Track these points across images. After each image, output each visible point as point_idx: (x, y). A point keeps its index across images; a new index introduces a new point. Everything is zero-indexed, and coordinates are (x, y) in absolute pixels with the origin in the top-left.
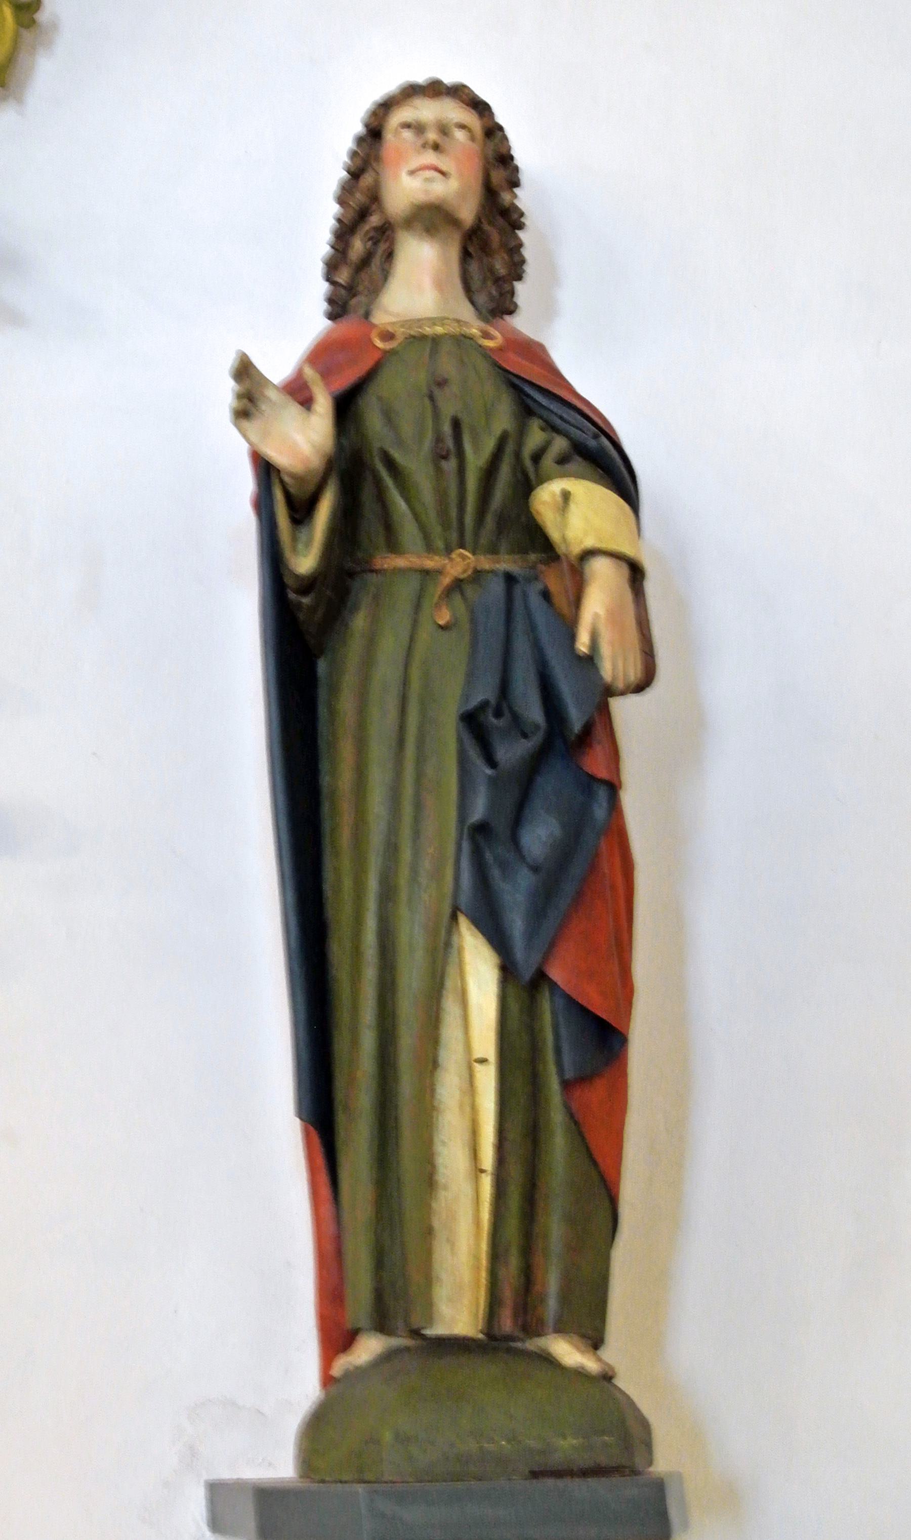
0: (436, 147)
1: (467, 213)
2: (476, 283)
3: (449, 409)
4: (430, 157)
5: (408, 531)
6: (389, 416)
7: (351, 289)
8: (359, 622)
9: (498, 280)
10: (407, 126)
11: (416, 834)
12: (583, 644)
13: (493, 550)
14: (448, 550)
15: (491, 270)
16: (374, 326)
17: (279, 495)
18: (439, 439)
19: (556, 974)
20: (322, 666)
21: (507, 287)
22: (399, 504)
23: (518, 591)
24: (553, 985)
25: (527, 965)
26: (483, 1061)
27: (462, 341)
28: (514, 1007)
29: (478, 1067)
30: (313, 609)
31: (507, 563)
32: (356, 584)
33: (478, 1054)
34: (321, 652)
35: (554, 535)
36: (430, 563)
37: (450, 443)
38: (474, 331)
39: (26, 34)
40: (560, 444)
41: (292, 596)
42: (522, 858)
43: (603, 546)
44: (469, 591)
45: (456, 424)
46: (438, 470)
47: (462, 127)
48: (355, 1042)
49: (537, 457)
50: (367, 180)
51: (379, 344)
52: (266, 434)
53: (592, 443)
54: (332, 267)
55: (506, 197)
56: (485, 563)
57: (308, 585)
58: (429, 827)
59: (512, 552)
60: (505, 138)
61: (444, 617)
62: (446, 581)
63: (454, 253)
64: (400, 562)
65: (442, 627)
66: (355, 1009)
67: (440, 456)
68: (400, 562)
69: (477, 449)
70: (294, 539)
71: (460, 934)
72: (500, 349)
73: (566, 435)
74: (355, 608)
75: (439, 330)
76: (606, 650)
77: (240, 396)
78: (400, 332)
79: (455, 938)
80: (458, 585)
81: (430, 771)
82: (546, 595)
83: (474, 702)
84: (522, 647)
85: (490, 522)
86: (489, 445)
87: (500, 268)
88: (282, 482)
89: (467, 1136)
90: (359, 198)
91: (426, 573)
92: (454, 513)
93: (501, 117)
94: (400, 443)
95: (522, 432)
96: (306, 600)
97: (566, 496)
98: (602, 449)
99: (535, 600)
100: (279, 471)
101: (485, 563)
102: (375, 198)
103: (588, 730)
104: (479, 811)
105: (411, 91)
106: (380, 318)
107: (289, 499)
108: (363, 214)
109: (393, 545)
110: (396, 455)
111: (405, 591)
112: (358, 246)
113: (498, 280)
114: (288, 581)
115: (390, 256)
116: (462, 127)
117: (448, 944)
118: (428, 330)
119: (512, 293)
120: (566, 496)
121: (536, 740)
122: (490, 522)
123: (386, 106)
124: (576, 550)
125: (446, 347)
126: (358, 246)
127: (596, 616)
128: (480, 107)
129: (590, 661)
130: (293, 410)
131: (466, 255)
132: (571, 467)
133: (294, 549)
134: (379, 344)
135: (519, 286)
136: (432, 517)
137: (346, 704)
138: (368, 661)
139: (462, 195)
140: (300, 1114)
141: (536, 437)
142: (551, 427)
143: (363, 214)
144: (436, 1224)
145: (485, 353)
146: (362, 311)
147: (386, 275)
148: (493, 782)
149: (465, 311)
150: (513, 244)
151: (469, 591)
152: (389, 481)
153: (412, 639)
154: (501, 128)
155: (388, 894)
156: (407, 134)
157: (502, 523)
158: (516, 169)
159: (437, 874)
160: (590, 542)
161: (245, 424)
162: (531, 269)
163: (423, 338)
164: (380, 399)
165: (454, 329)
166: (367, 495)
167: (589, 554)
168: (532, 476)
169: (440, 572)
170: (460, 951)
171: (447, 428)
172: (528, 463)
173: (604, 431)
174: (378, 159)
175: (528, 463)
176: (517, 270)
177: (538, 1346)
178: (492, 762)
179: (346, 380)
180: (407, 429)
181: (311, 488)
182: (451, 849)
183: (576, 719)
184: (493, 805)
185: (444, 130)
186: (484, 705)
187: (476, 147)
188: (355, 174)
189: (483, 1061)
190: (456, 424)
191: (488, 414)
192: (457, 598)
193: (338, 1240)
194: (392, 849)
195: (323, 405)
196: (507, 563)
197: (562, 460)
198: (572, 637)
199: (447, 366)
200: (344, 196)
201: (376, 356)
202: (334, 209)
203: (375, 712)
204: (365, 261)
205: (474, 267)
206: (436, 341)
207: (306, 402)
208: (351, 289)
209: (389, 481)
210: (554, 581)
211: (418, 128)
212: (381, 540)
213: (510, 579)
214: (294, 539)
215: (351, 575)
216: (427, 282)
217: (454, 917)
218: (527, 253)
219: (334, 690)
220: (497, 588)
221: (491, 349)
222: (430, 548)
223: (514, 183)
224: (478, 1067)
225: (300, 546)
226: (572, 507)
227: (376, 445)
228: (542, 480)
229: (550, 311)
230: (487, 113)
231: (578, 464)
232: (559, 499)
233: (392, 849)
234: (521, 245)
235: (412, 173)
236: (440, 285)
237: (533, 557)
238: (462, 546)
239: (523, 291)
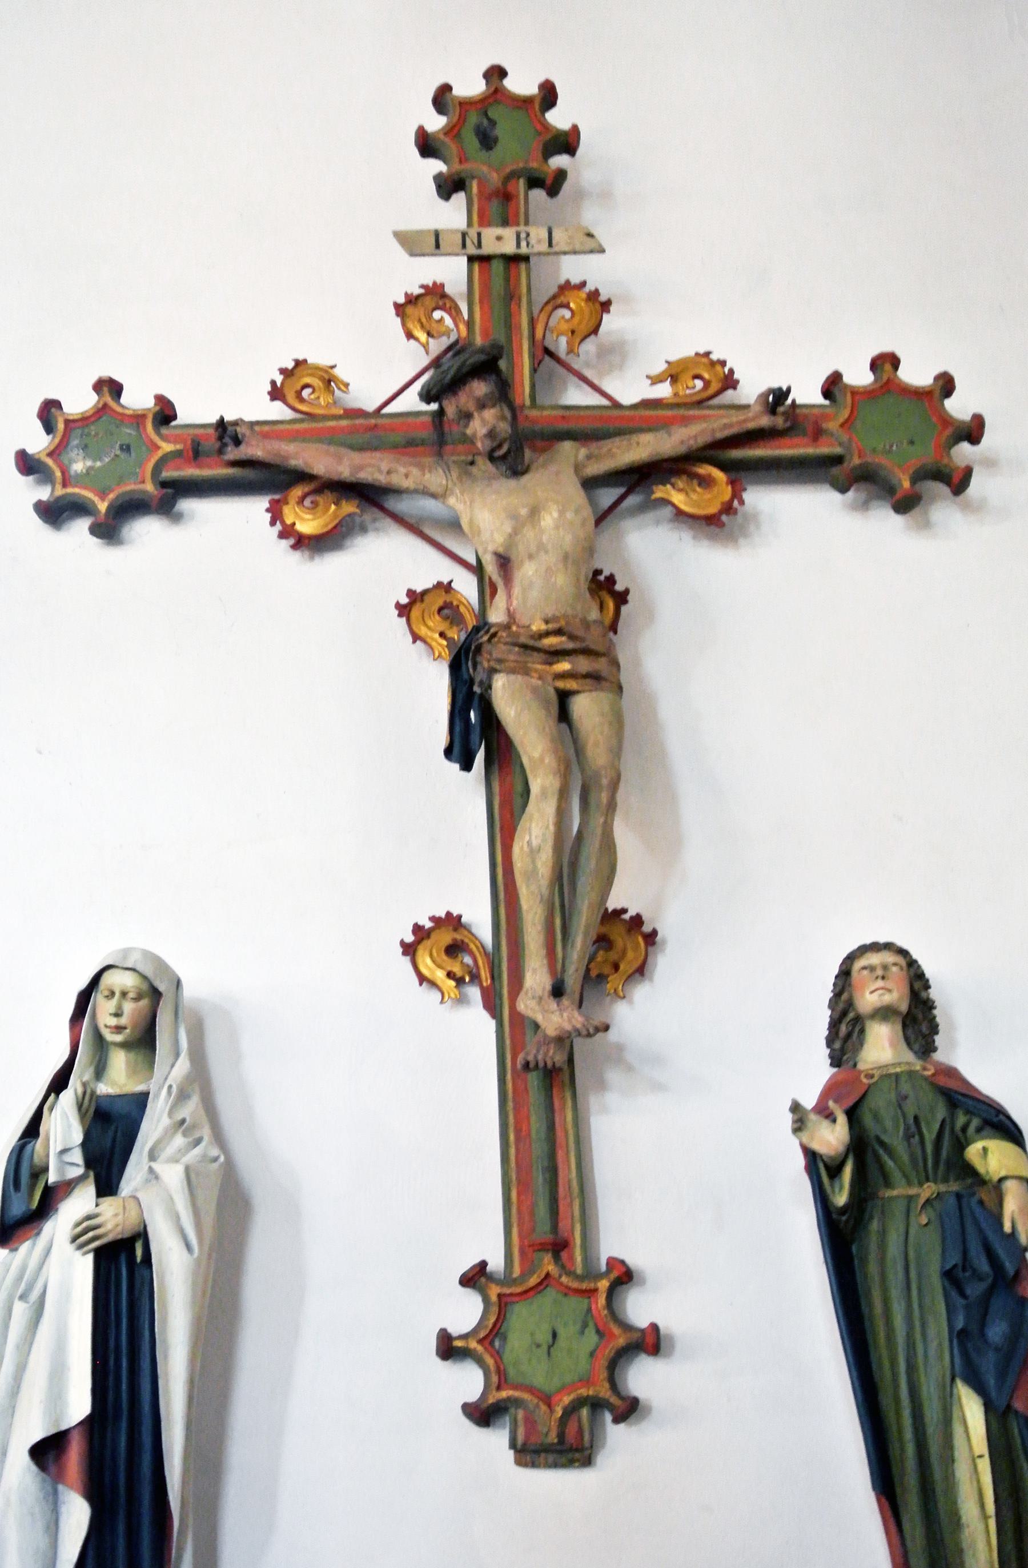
0: (883, 978)
1: (904, 1007)
2: (912, 1037)
3: (911, 1110)
4: (880, 983)
5: (896, 1175)
6: (876, 1117)
7: (843, 1051)
8: (875, 1225)
9: (924, 1036)
10: (864, 968)
11: (924, 1335)
12: (1007, 1227)
13: (945, 1180)
14: (921, 1184)
15: (921, 1031)
16: (860, 1072)
17: (821, 1166)
18: (907, 1128)
19: (1018, 1405)
20: (854, 1249)
21: (930, 1040)
22: (890, 1163)
23: (965, 1200)
24: (1016, 1412)
25: (1002, 1404)
26: (981, 1456)
27: (911, 1074)
28: (994, 1425)
29: (979, 1461)
30: (847, 1221)
31: (954, 1187)
32: (870, 1204)
33: (977, 1453)
34: (852, 1242)
35: (981, 1170)
36: (913, 1191)
37: (913, 1128)
38: (918, 1068)
39: (650, 949)
40: (975, 1122)
41: (834, 1216)
42: (986, 1342)
43: (1011, 1173)
44: (936, 1204)
45: (916, 1119)
46: (909, 1145)
47: (895, 964)
48: (903, 1449)
49: (964, 1129)
50: (845, 996)
51: (865, 1081)
52: (812, 1138)
53: (995, 1120)
54: (830, 1042)
55: (924, 995)
56: (943, 1188)
57: (843, 1210)
58: (932, 1332)
59: (956, 1180)
60: (919, 967)
61: (924, 1220)
62: (922, 1201)
63: (899, 1027)
64: (895, 1193)
65: (926, 1225)
66: (900, 1431)
67: (908, 1137)
68: (895, 1193)
69: (929, 1132)
70: (832, 1186)
71: (957, 1387)
72: (933, 1075)
73: (979, 1116)
74: (871, 1218)
75: (898, 1070)
76: (1021, 1229)
77: (794, 1122)
78: (877, 1074)
79: (955, 1391)
80: (928, 1201)
81: (927, 1301)
82: (981, 1202)
83: (948, 1267)
84: (970, 1229)
85: (942, 1167)
86: (937, 1126)
87: (924, 1029)
88: (823, 1160)
89: (977, 1497)
90: (841, 1006)
91: (910, 1199)
92: (921, 1164)
93: (915, 955)
94: (885, 1131)
95: (953, 1117)
96: (844, 1218)
97: (985, 1150)
98: (1000, 1121)
99: (978, 1210)
100: (821, 1156)
101: (943, 1188)
102: (850, 1004)
103: (1017, 1274)
104: (960, 1324)
105: (864, 950)
106: (861, 1066)
107: (827, 1167)
108: (844, 1014)
109: (888, 1184)
110: (885, 1138)
111: (899, 1209)
112: (843, 1029)
113: (924, 1036)
114: (831, 1209)
115: (862, 1031)
116: (895, 964)
117: (951, 1395)
118: (892, 1071)
119: (934, 1041)
120: (985, 1150)
121: (990, 1280)
122: (942, 1167)
123: (851, 959)
124: (995, 1178)
125: (903, 1079)
126: (843, 1029)
127: (1013, 1212)
128: (903, 953)
129: (1013, 1234)
130: (825, 1124)
131: (905, 1026)
132: (985, 1133)
133: (833, 1192)
134: (865, 1081)
135: (937, 1038)
136: (908, 1168)
137: (873, 1268)
138: (883, 1246)
139: (900, 999)
140: (874, 1488)
141: (961, 1119)
142: (968, 1112)
143: (844, 1014)
144: (965, 1545)
145: (926, 1079)
146: (851, 1063)
147: (861, 1044)
148: (967, 1307)
149: (909, 1056)
150: (931, 1017)
151: (936, 1204)
152: (881, 1152)
153: (907, 1233)
154: (916, 961)
155: (911, 1368)
156: (865, 972)
157: (949, 1165)
158: (928, 981)
159: (941, 1358)
160: (1003, 1173)
161: (799, 1134)
162: (941, 1028)
163: (889, 1076)
164: (870, 1110)
165: (904, 1068)
166: (869, 1158)
167: (1001, 1180)
168: (963, 1140)
169: (918, 1196)
170: (959, 1399)
171: (911, 1121)
172: (960, 1134)
173: (999, 1111)
174: (850, 985)
175: (960, 1134)
176: (934, 1029)
177: (600, 1340)
178: (963, 1294)
179: (850, 1102)
180: (889, 1124)
181: (841, 1159)
182: (946, 1344)
183: (1010, 1268)
184: (968, 1317)
185: (885, 967)
186: (955, 1266)
187: (904, 973)
188: (838, 994)
189: (981, 1456)
190: (916, 1119)
191: (932, 1110)
192: (929, 1210)
193: (905, 1554)
194: (911, 1345)
195: (842, 1119)
196: (954, 1187)
197: (979, 1130)
198: (1001, 1225)
199: (905, 1087)
200: (833, 1004)
201: (866, 1087)
202: (829, 1012)
203: (891, 1276)
204: (849, 1035)
205: (910, 1032)
206: (897, 1076)
207: (831, 1118)
208: (843, 1051)
209: (881, 1152)
210: (983, 1194)
211: (872, 968)
212: (881, 1181)
213: (959, 1196)
214: (832, 1186)
215: (865, 1200)
216: (887, 1044)
217: (953, 1379)
218: (938, 1019)
219: (864, 1260)
220: (952, 1201)
221: (929, 1076)
222: (909, 1183)
223: (927, 986)
224: (979, 1461)
225: (837, 1190)
226: (990, 1155)
227: (872, 1134)
228: (968, 1144)
229: (953, 1044)
230: (908, 956)
231: (988, 1131)
232: (981, 1151)
233: (911, 1345)
234: (935, 1017)
235: (872, 992)
236: (893, 1045)
237: (969, 1181)
238: (928, 1180)
239: (938, 1040)
